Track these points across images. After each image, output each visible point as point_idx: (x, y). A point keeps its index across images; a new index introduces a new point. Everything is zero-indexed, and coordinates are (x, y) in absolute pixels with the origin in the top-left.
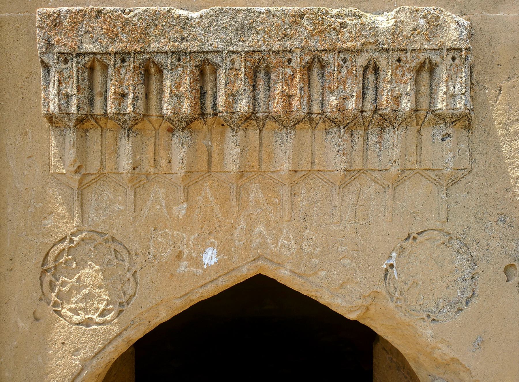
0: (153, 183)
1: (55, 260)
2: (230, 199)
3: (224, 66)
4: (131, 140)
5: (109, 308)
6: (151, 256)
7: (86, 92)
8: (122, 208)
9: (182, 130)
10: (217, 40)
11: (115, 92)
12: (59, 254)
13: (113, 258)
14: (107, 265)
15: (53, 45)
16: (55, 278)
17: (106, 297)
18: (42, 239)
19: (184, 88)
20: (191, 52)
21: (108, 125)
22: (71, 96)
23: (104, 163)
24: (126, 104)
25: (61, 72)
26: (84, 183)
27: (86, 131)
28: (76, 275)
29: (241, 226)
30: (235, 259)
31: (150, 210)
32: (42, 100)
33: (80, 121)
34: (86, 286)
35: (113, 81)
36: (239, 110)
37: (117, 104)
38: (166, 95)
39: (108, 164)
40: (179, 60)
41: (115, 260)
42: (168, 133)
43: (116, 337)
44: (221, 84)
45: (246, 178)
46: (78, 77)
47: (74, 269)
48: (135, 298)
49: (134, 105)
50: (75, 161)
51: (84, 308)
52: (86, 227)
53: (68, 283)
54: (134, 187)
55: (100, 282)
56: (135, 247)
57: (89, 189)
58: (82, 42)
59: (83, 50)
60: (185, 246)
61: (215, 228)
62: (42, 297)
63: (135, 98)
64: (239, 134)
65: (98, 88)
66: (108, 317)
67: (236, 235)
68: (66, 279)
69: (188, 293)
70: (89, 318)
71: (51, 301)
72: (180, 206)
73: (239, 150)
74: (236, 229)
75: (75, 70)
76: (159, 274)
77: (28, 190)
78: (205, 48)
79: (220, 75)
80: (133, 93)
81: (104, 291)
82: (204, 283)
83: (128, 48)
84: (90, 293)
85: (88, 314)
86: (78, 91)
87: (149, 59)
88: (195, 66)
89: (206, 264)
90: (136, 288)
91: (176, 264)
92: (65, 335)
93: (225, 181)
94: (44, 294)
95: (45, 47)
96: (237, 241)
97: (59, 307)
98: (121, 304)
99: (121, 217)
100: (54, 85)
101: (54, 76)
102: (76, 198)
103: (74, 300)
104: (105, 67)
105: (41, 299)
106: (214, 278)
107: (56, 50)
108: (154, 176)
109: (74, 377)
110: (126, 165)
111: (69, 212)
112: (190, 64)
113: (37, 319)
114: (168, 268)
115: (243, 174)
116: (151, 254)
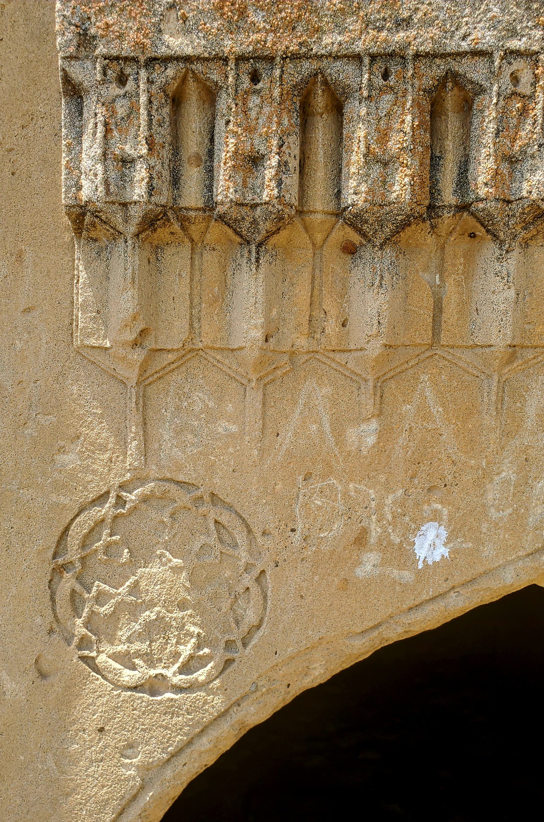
0: (303, 374)
1: (83, 546)
2: (480, 413)
3: (495, 88)
4: (262, 270)
5: (201, 653)
6: (298, 536)
7: (166, 153)
8: (234, 428)
9: (382, 245)
10: (481, 25)
11: (236, 152)
12: (91, 530)
13: (213, 540)
14: (197, 555)
15: (94, 37)
16: (81, 584)
17: (196, 630)
18: (54, 498)
19: (394, 144)
20: (417, 56)
21: (208, 236)
22: (133, 161)
23: (196, 325)
24: (259, 181)
25: (110, 105)
26: (153, 367)
27: (157, 249)
28: (128, 578)
29: (504, 474)
30: (488, 551)
31: (295, 434)
32: (64, 172)
33: (151, 222)
34: (151, 605)
35: (231, 126)
36: (524, 194)
37: (240, 181)
38: (354, 158)
39: (206, 328)
40: (386, 76)
41: (219, 545)
42: (343, 255)
43: (215, 719)
44: (484, 132)
45: (520, 362)
46: (149, 115)
47: (124, 564)
48: (260, 633)
49: (280, 183)
50: (134, 319)
51: (146, 654)
52: (153, 471)
53: (112, 596)
54: (262, 382)
55: (183, 594)
56: (262, 516)
57: (161, 385)
58: (160, 31)
59: (164, 49)
60: (374, 518)
61: (442, 478)
62: (55, 626)
63: (283, 165)
64: (515, 254)
65: (193, 144)
66: (201, 675)
67: (490, 496)
68: (108, 588)
69: (379, 625)
70: (156, 676)
71: (74, 635)
72: (364, 427)
73: (511, 294)
74: (491, 481)
75: (143, 99)
76: (316, 578)
77: (24, 385)
78: (451, 46)
79: (482, 111)
80: (278, 154)
81: (191, 616)
82: (417, 603)
83: (269, 44)
84: (160, 618)
85: (154, 667)
86: (150, 149)
87: (316, 75)
88: (424, 90)
89: (422, 559)
90: (265, 609)
91: (354, 557)
92: (105, 712)
93: (470, 370)
94: (57, 621)
95: (75, 42)
96: (493, 510)
97: (91, 649)
98: (229, 645)
99: (231, 450)
100: (94, 134)
101: (95, 112)
102: (133, 405)
103: (123, 634)
104: (210, 94)
105: (51, 631)
106: (441, 591)
107: (101, 50)
108: (306, 357)
109: (124, 802)
110: (248, 328)
111: (116, 436)
112: (412, 85)
113: (43, 675)
114: (335, 566)
115: (515, 352)
116: (298, 532)
